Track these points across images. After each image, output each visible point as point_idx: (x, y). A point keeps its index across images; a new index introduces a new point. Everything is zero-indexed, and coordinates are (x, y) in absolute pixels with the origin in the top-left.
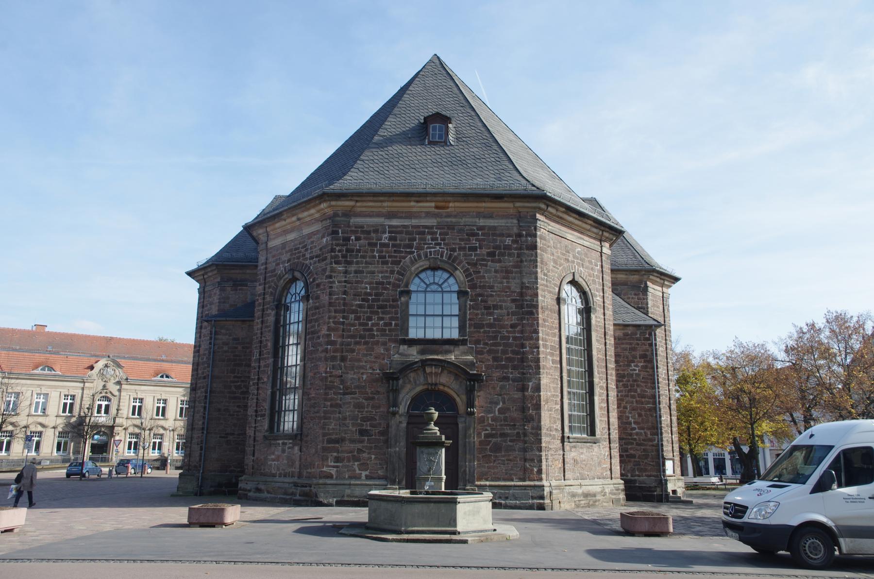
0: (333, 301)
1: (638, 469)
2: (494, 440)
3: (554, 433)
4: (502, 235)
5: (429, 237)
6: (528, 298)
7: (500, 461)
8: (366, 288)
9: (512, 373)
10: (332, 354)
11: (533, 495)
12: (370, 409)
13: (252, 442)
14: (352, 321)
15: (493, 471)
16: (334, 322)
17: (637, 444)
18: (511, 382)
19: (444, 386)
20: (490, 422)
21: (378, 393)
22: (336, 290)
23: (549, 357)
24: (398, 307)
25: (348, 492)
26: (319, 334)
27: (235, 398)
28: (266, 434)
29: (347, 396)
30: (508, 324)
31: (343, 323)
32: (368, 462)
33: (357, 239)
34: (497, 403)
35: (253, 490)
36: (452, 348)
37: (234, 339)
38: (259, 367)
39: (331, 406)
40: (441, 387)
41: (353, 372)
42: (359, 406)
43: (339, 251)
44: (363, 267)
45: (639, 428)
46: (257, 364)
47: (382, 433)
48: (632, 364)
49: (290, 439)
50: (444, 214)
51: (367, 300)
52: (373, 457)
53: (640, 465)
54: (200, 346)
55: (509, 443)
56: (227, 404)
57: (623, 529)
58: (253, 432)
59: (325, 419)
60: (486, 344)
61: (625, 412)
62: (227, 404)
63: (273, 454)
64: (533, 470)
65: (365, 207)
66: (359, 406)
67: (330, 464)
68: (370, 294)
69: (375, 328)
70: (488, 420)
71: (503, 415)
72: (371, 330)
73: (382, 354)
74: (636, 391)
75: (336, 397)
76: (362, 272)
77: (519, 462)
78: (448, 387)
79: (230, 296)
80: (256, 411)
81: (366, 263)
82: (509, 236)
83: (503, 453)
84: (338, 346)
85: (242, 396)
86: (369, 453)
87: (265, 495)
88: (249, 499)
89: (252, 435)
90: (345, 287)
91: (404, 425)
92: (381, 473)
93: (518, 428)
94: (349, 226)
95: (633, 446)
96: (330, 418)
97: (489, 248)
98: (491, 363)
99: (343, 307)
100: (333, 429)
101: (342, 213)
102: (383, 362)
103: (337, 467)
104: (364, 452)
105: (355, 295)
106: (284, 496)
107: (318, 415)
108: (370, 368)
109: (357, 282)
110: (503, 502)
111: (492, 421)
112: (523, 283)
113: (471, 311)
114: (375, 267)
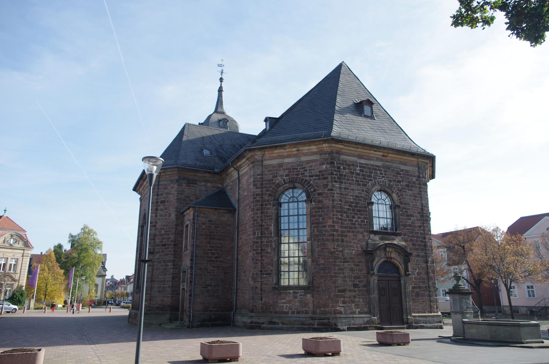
2: (416, 290)
4: (411, 176)
5: (379, 172)
7: (420, 302)
9: (421, 253)
10: (337, 237)
11: (437, 321)
12: (357, 272)
14: (345, 218)
16: (336, 218)
20: (414, 280)
21: (361, 262)
25: (352, 322)
26: (325, 225)
27: (211, 261)
29: (345, 264)
32: (359, 303)
33: (344, 168)
34: (416, 270)
36: (394, 237)
37: (210, 221)
38: (262, 242)
39: (339, 269)
43: (336, 175)
44: (348, 186)
47: (365, 286)
50: (385, 160)
52: (361, 300)
54: (156, 223)
56: (206, 265)
57: (378, 341)
58: (260, 285)
59: (335, 277)
60: (408, 236)
62: (206, 265)
63: (284, 299)
64: (434, 307)
65: (348, 150)
66: (352, 270)
68: (353, 203)
69: (356, 223)
70: (413, 279)
76: (348, 189)
78: (396, 260)
79: (185, 190)
81: (350, 184)
82: (415, 177)
84: (339, 233)
85: (215, 260)
86: (359, 298)
87: (280, 325)
88: (263, 329)
90: (341, 197)
91: (376, 281)
92: (366, 310)
93: (426, 284)
94: (339, 160)
96: (338, 277)
97: (406, 182)
101: (336, 152)
102: (362, 243)
104: (357, 297)
105: (345, 202)
106: (302, 326)
108: (356, 247)
109: (346, 195)
110: (425, 325)
112: (422, 203)
114: (354, 187)
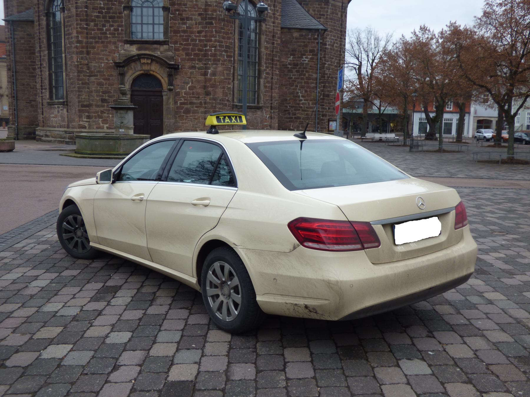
0: (79, 13)
1: (301, 126)
2: (186, 106)
3: (226, 102)
6: (210, 13)
8: (101, 4)
9: (198, 64)
10: (80, 50)
13: (41, 106)
14: (93, 27)
15: (185, 125)
17: (303, 111)
18: (197, 70)
19: (153, 71)
21: (112, 75)
22: (80, 5)
23: (224, 53)
24: (123, 18)
28: (49, 101)
29: (92, 78)
30: (195, 31)
31: (86, 29)
32: (108, 119)
34: (188, 83)
35: (44, 136)
36: (158, 46)
37: (28, 35)
39: (83, 84)
40: (152, 73)
41: (95, 62)
42: (100, 84)
45: (305, 100)
46: (39, 54)
48: (304, 57)
49: (61, 105)
51: (102, 13)
53: (303, 124)
55: (196, 109)
56: (28, 81)
60: (181, 44)
61: (296, 89)
62: (28, 81)
63: (53, 113)
66: (100, 84)
67: (84, 120)
68: (103, 8)
69: (108, 32)
70: (182, 94)
71: (192, 91)
72: (106, 33)
73: (113, 50)
74: (305, 75)
75: (85, 78)
77: (201, 120)
80: (42, 86)
83: (191, 115)
86: (108, 114)
87: (50, 139)
88: (42, 141)
89: (41, 101)
93: (201, 99)
95: (300, 112)
96: (82, 92)
98: (184, 57)
99: (85, 17)
100: (85, 98)
103: (89, 122)
104: (105, 113)
107: (75, 89)
111: (184, 94)
113: (172, 21)
